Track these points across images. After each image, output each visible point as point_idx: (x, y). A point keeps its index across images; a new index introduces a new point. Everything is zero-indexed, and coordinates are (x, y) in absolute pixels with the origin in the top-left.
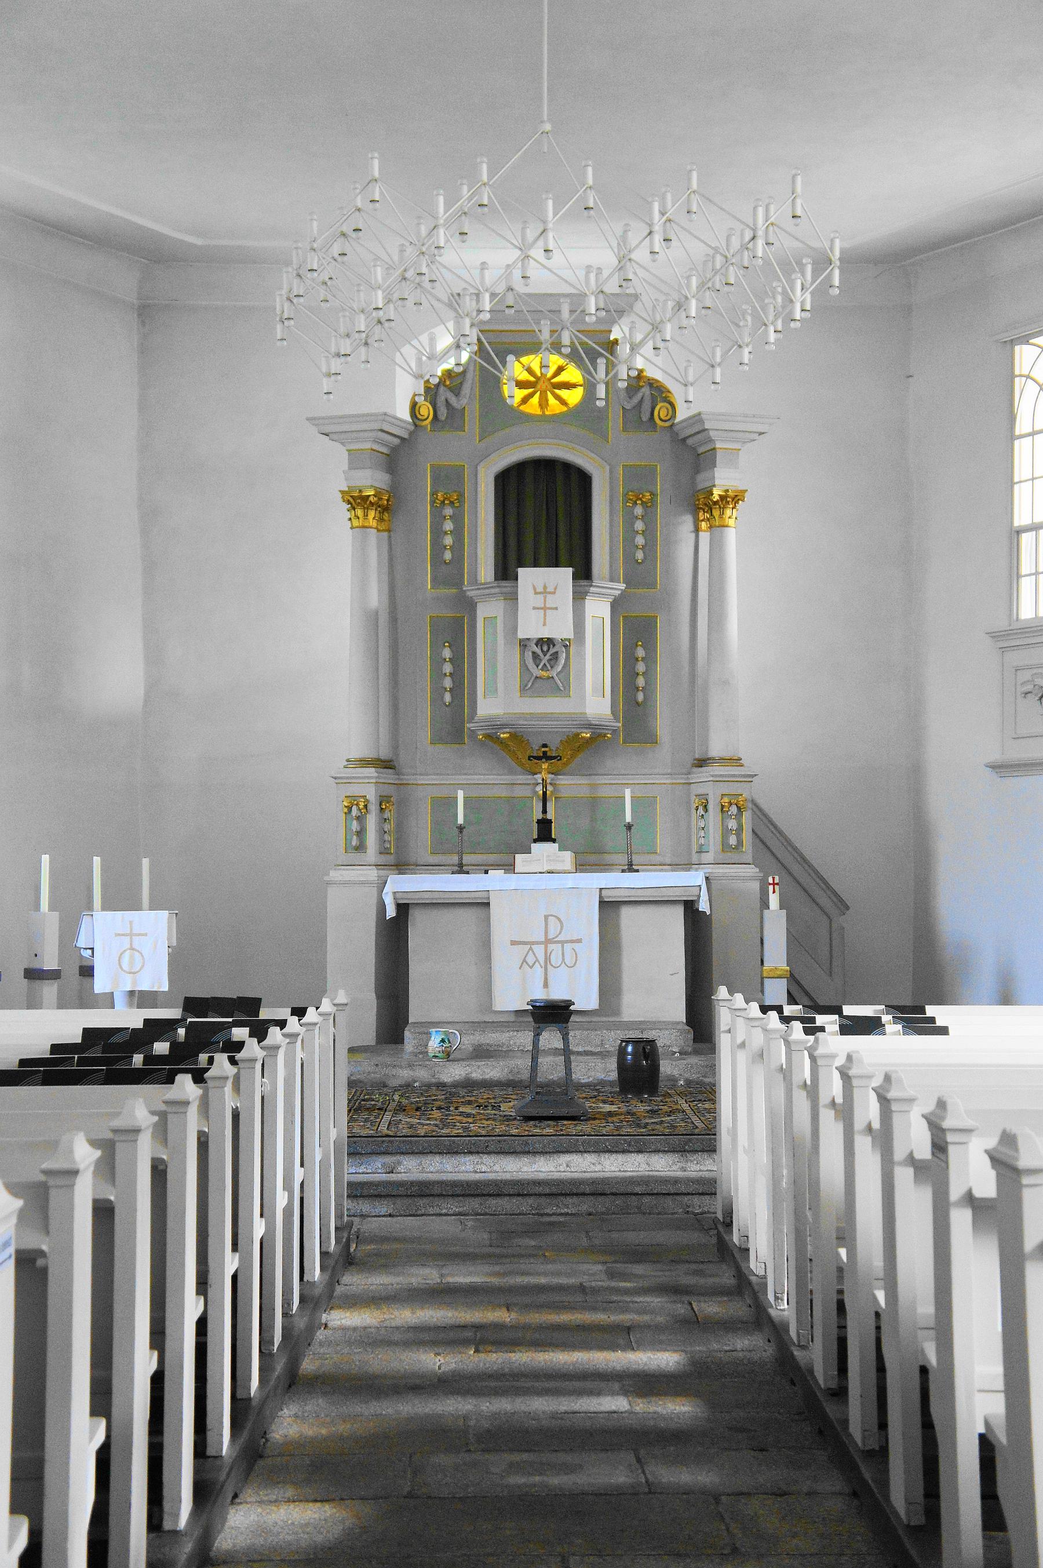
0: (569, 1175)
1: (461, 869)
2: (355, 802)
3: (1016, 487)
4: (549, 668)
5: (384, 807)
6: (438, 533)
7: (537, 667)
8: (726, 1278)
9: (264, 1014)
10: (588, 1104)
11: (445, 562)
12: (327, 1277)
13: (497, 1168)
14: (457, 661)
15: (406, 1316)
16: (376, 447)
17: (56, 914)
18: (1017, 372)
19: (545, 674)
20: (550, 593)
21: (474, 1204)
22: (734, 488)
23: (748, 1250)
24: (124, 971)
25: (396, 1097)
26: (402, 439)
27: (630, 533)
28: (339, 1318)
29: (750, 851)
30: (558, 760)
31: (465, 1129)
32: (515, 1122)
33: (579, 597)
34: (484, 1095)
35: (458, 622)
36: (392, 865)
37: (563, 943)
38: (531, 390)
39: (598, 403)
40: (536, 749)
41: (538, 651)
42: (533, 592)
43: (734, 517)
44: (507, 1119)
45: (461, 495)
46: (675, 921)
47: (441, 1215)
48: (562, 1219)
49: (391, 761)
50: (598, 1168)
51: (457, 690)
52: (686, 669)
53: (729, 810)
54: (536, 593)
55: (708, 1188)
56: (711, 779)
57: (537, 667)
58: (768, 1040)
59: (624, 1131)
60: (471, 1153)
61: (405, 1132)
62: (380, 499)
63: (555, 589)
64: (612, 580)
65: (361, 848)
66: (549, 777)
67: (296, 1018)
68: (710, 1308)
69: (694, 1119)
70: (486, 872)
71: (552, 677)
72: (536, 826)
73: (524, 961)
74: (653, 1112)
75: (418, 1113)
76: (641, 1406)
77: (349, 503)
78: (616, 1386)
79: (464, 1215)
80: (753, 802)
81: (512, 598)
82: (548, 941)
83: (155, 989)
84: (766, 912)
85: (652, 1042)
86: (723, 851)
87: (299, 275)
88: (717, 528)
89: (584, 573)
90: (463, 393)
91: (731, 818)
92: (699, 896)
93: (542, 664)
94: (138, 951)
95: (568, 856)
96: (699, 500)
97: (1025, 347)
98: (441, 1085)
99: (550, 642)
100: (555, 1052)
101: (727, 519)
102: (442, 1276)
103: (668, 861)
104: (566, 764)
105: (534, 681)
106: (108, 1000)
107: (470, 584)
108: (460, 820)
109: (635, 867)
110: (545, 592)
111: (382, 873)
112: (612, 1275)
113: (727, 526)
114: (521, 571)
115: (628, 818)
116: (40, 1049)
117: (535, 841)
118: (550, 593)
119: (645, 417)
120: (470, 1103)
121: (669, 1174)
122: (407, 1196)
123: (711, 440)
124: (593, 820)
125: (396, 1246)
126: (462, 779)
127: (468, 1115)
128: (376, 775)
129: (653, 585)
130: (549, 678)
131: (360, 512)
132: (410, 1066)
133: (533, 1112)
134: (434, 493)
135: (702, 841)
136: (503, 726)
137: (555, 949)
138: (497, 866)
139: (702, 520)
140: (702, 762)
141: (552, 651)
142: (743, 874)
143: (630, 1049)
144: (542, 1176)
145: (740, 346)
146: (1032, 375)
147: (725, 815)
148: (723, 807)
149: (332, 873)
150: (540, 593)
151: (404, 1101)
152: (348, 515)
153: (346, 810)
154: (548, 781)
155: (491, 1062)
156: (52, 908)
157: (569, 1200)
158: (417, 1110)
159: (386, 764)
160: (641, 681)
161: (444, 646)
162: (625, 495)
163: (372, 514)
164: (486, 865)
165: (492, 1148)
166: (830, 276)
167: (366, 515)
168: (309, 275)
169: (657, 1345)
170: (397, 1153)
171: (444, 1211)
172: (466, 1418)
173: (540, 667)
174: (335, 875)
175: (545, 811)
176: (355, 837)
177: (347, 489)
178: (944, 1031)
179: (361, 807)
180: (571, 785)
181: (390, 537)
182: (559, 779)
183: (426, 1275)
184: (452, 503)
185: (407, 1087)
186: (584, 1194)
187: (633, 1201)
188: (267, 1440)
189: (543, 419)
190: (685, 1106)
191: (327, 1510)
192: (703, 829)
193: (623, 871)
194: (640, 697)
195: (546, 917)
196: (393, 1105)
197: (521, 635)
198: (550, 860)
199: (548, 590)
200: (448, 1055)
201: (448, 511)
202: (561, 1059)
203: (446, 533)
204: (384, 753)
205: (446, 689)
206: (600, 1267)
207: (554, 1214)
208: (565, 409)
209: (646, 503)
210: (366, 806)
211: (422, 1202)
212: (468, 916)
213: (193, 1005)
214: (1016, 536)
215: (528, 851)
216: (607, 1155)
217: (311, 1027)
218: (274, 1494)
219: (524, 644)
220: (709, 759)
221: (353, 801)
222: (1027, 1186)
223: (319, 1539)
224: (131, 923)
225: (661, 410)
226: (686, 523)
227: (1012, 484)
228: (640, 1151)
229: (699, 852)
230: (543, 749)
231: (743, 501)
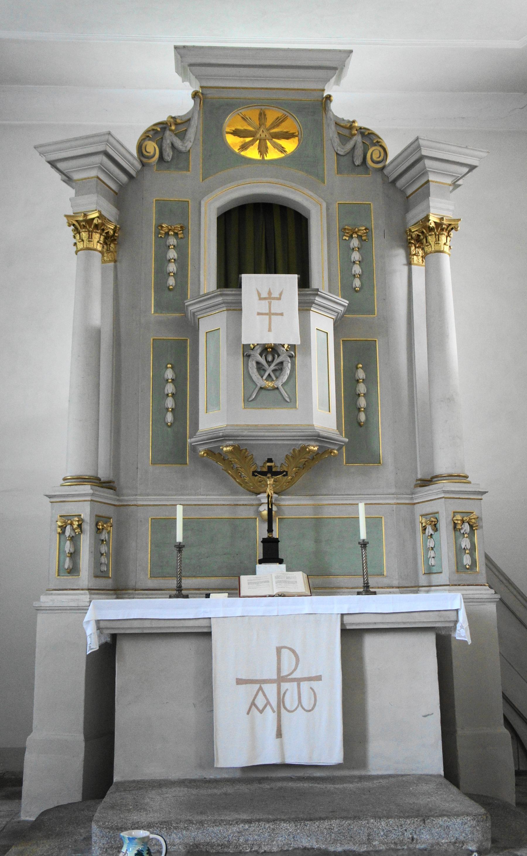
2: (69, 522)
4: (274, 379)
5: (101, 527)
7: (262, 377)
11: (169, 288)
19: (270, 384)
20: (274, 299)
30: (284, 476)
36: (109, 590)
37: (299, 681)
40: (260, 463)
41: (262, 361)
42: (256, 297)
53: (462, 528)
54: (261, 299)
56: (442, 495)
57: (262, 377)
63: (281, 294)
65: (74, 570)
71: (277, 388)
73: (253, 704)
82: (281, 679)
86: (457, 571)
90: (187, 137)
91: (464, 537)
92: (456, 622)
101: (442, 246)
103: (395, 583)
105: (259, 391)
108: (179, 538)
110: (270, 298)
113: (443, 252)
114: (245, 277)
117: (261, 562)
118: (274, 299)
119: (358, 162)
124: (317, 541)
128: (91, 491)
129: (372, 312)
131: (84, 235)
136: (225, 438)
137: (289, 687)
138: (220, 590)
139: (415, 255)
142: (481, 596)
148: (455, 525)
149: (43, 598)
150: (265, 299)
153: (59, 530)
161: (167, 368)
164: (208, 589)
173: (264, 377)
174: (46, 600)
176: (68, 559)
177: (72, 214)
179: (75, 526)
181: (115, 267)
182: (283, 500)
184: (176, 234)
189: (263, 162)
192: (432, 549)
193: (359, 593)
194: (362, 417)
195: (279, 650)
197: (244, 341)
198: (280, 582)
199: (273, 296)
201: (172, 241)
204: (103, 474)
209: (361, 236)
210: (80, 526)
215: (254, 573)
219: (246, 347)
220: (436, 477)
221: (67, 520)
225: (374, 152)
226: (400, 255)
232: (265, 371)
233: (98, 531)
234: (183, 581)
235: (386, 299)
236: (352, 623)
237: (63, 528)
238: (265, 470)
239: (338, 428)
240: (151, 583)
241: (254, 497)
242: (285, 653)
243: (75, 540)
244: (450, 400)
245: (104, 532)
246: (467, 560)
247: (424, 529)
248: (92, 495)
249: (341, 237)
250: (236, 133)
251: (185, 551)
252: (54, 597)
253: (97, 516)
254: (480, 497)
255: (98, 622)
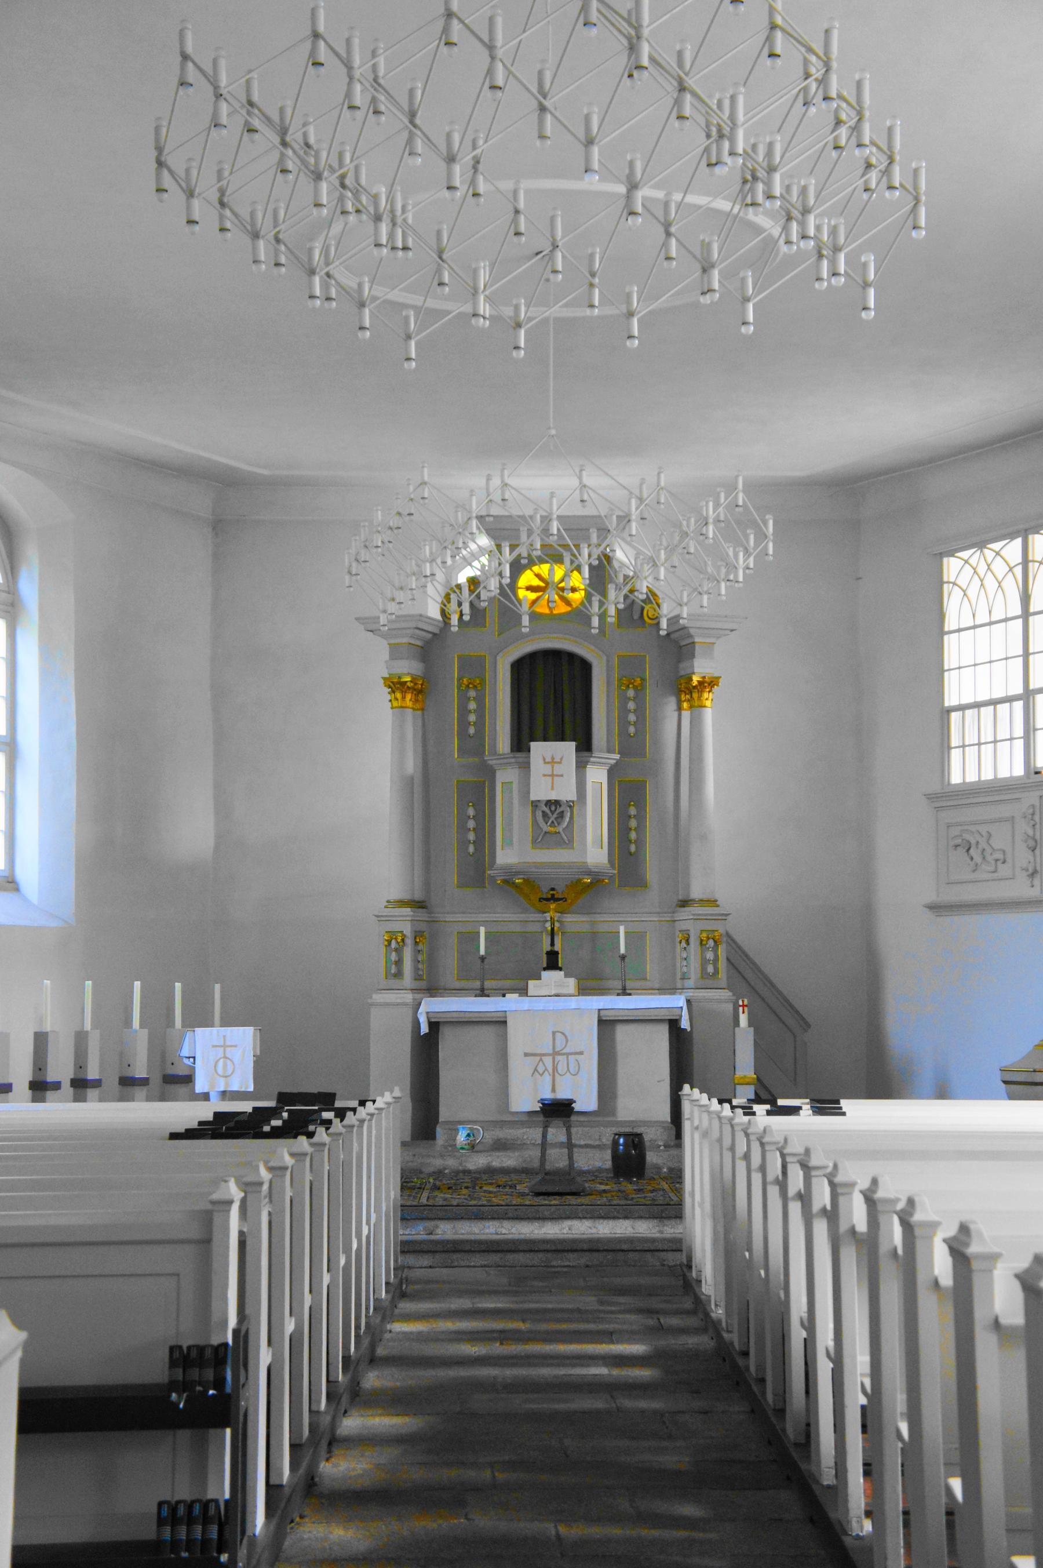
0: (571, 1236)
1: (483, 993)
3: (946, 674)
6: (464, 712)
8: (688, 1304)
9: (338, 1104)
10: (587, 1185)
12: (390, 1296)
13: (514, 1230)
14: (479, 818)
15: (449, 1325)
16: (413, 642)
17: (146, 1031)
18: (945, 579)
19: (552, 829)
20: (556, 763)
21: (495, 1258)
22: (710, 676)
23: (700, 1281)
24: (220, 1076)
25: (431, 1180)
26: (434, 634)
27: (624, 711)
28: (398, 1327)
29: (725, 979)
31: (489, 1201)
32: (529, 1197)
33: (581, 766)
34: (502, 1179)
35: (479, 787)
37: (568, 1054)
38: (540, 594)
39: (593, 631)
41: (546, 810)
42: (541, 761)
43: (710, 699)
44: (523, 1195)
45: (483, 682)
46: (661, 1037)
47: (468, 1267)
48: (565, 1270)
49: (423, 902)
50: (594, 1231)
51: (479, 843)
52: (671, 825)
54: (545, 763)
55: (677, 1245)
56: (692, 917)
58: (710, 1119)
59: (615, 1202)
60: (493, 1219)
61: (440, 1203)
62: (416, 684)
64: (609, 751)
65: (399, 975)
66: (556, 916)
67: (339, 1120)
68: (674, 1321)
69: (671, 1195)
70: (504, 996)
71: (559, 833)
72: (545, 956)
73: (536, 1070)
74: (640, 1190)
75: (450, 1191)
76: (616, 1372)
77: (390, 687)
78: (601, 1362)
79: (489, 1267)
80: (728, 934)
81: (526, 766)
82: (555, 1053)
83: (243, 1089)
84: (736, 1029)
85: (639, 1136)
87: (366, 547)
88: (697, 707)
89: (585, 746)
93: (550, 822)
94: (231, 1060)
95: (571, 984)
96: (681, 684)
97: (952, 559)
98: (467, 1172)
99: (557, 803)
100: (561, 1145)
102: (473, 1303)
103: (657, 986)
104: (571, 904)
106: (206, 1097)
107: (489, 754)
109: (628, 991)
110: (553, 762)
111: (418, 996)
112: (601, 1302)
113: (705, 707)
114: (533, 745)
115: (622, 950)
116: (194, 1125)
117: (545, 969)
118: (556, 763)
119: (636, 616)
120: (491, 1184)
121: (649, 1235)
122: (444, 1251)
123: (690, 636)
125: (435, 1286)
126: (482, 917)
127: (490, 1192)
128: (412, 913)
129: (643, 755)
130: (556, 833)
131: (399, 695)
132: (442, 1156)
133: (543, 1189)
134: (460, 679)
135: (685, 969)
136: (517, 873)
138: (513, 990)
140: (684, 903)
141: (559, 810)
143: (621, 1141)
144: (549, 1237)
145: (700, 594)
146: (958, 582)
147: (704, 947)
148: (702, 941)
149: (375, 996)
150: (548, 763)
151: (438, 1183)
152: (389, 697)
153: (386, 943)
154: (556, 919)
155: (509, 1153)
156: (141, 1027)
157: (571, 1255)
158: (449, 1188)
159: (419, 905)
160: (633, 835)
161: (469, 806)
162: (620, 680)
163: (409, 696)
165: (510, 1215)
166: (766, 547)
167: (404, 698)
168: (375, 550)
169: (629, 1341)
170: (435, 1219)
171: (472, 1264)
172: (495, 1378)
174: (378, 998)
175: (552, 944)
176: (393, 966)
177: (388, 676)
178: (844, 1114)
179: (399, 940)
180: (575, 922)
181: (423, 714)
182: (566, 917)
183: (465, 1303)
184: (475, 687)
185: (439, 1173)
186: (583, 1250)
187: (620, 1256)
188: (360, 1388)
190: (666, 1186)
191: (407, 1419)
192: (685, 959)
193: (618, 995)
194: (633, 848)
195: (554, 1033)
196: (428, 1186)
197: (533, 797)
200: (473, 1147)
201: (472, 693)
202: (566, 1151)
203: (470, 711)
204: (418, 896)
205: (470, 841)
206: (593, 1298)
207: (558, 1267)
208: (569, 609)
209: (637, 687)
210: (403, 940)
211: (455, 1256)
212: (488, 1033)
213: (284, 1098)
214: (946, 716)
216: (601, 1221)
217: (278, 1173)
218: (370, 1412)
219: (535, 804)
220: (691, 900)
221: (392, 935)
222: (843, 1194)
223: (404, 1431)
224: (224, 1037)
226: (671, 703)
227: (943, 671)
228: (626, 1218)
229: (683, 979)
230: (552, 892)
231: (718, 685)
232: (549, 818)
233: (416, 943)
234: (486, 983)
235: (657, 742)
236: (607, 1016)
237: (389, 942)
238: (550, 896)
239: (609, 861)
240: (458, 984)
241: (541, 915)
242: (558, 1035)
243: (399, 951)
244: (703, 838)
245: (420, 944)
246: (710, 969)
247: (680, 942)
248: (413, 916)
249: (619, 687)
250: (530, 588)
251: (486, 961)
252: (385, 995)
253: (416, 932)
254: (724, 918)
255: (427, 1013)
